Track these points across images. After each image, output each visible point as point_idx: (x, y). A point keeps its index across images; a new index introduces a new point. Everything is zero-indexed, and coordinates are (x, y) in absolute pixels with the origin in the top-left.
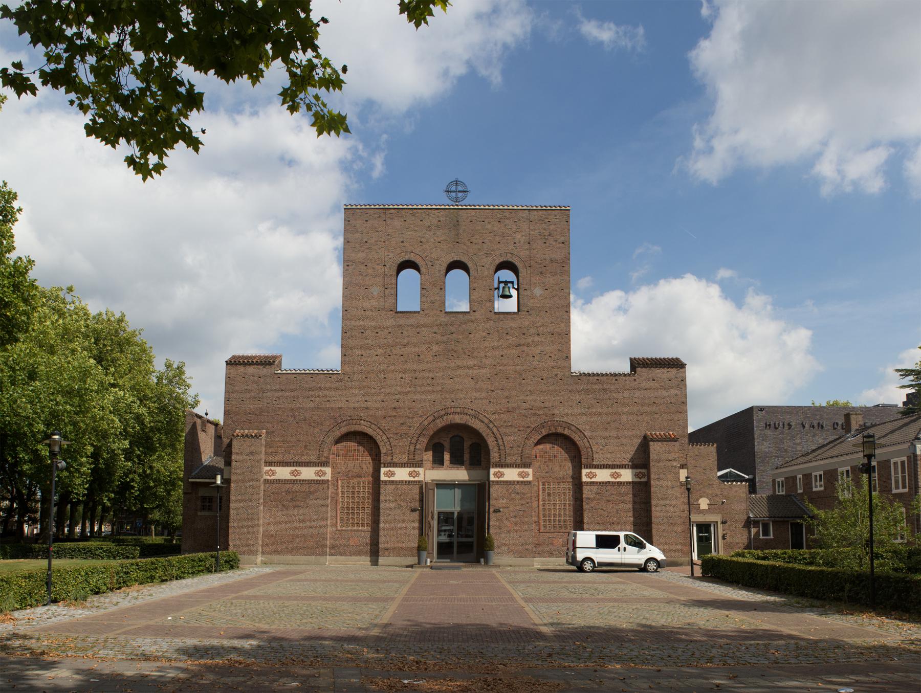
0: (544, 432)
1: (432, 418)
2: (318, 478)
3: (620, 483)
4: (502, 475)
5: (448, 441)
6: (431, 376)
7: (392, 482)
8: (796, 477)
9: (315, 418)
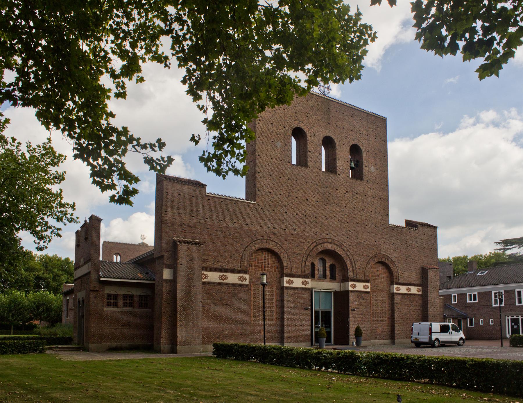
0: (376, 260)
1: (315, 244)
2: (241, 282)
4: (220, 277)
6: (315, 215)
9: (238, 235)
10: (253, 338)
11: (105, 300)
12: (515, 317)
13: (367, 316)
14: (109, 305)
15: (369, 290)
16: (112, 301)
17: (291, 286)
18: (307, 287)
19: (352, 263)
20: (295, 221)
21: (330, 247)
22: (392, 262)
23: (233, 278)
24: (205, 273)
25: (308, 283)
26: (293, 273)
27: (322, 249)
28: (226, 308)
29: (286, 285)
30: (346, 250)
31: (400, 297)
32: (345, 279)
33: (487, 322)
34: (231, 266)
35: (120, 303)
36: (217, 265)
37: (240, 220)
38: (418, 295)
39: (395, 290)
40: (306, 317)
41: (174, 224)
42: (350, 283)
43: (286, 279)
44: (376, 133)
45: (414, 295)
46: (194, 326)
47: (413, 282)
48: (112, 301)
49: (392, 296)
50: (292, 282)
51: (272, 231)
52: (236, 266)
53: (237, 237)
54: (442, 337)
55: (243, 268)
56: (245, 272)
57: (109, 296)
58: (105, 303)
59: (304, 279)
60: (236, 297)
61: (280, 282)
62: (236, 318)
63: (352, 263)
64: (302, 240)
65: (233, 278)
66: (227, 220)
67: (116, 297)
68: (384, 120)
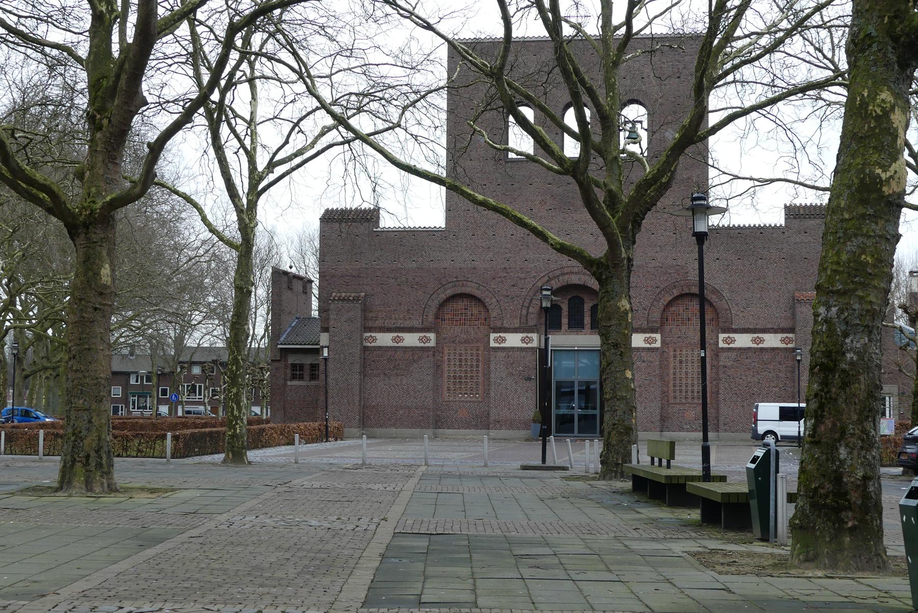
1: (546, 278)
2: (422, 345)
3: (762, 349)
4: (762, 341)
5: (566, 302)
10: (446, 421)
11: (289, 372)
13: (653, 389)
14: (294, 377)
16: (298, 373)
17: (502, 345)
20: (509, 246)
23: (411, 340)
25: (531, 340)
26: (505, 325)
27: (559, 285)
28: (401, 380)
29: (721, 345)
31: (733, 355)
34: (408, 324)
35: (307, 376)
36: (389, 323)
37: (422, 256)
40: (527, 391)
41: (334, 276)
44: (681, 67)
45: (773, 349)
46: (349, 404)
47: (770, 326)
48: (298, 373)
50: (523, 340)
51: (470, 266)
52: (416, 323)
53: (417, 284)
54: (781, 429)
56: (531, 330)
57: (294, 366)
58: (289, 376)
60: (415, 365)
62: (415, 392)
64: (523, 276)
65: (411, 340)
66: (402, 259)
67: (301, 367)
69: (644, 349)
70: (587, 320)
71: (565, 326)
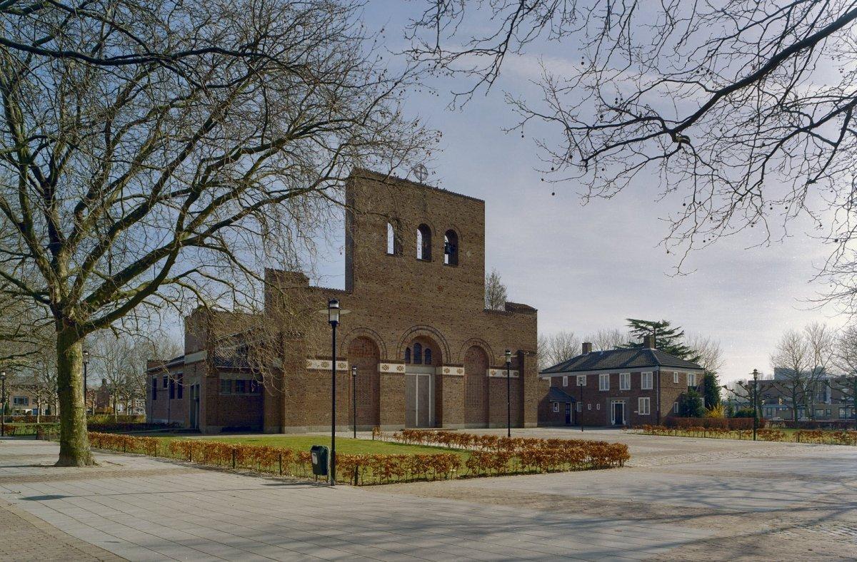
7: (387, 373)
8: (562, 378)
12: (619, 403)
15: (463, 374)
18: (401, 372)
19: (445, 348)
21: (424, 333)
22: (488, 346)
24: (309, 360)
25: (402, 368)
29: (382, 370)
30: (440, 336)
32: (440, 364)
33: (594, 407)
38: (515, 379)
39: (381, 368)
42: (444, 368)
43: (382, 365)
49: (487, 379)
50: (388, 368)
55: (343, 355)
59: (399, 365)
61: (376, 367)
63: (445, 348)
68: (483, 202)
69: (457, 376)
70: (423, 358)
71: (412, 361)
